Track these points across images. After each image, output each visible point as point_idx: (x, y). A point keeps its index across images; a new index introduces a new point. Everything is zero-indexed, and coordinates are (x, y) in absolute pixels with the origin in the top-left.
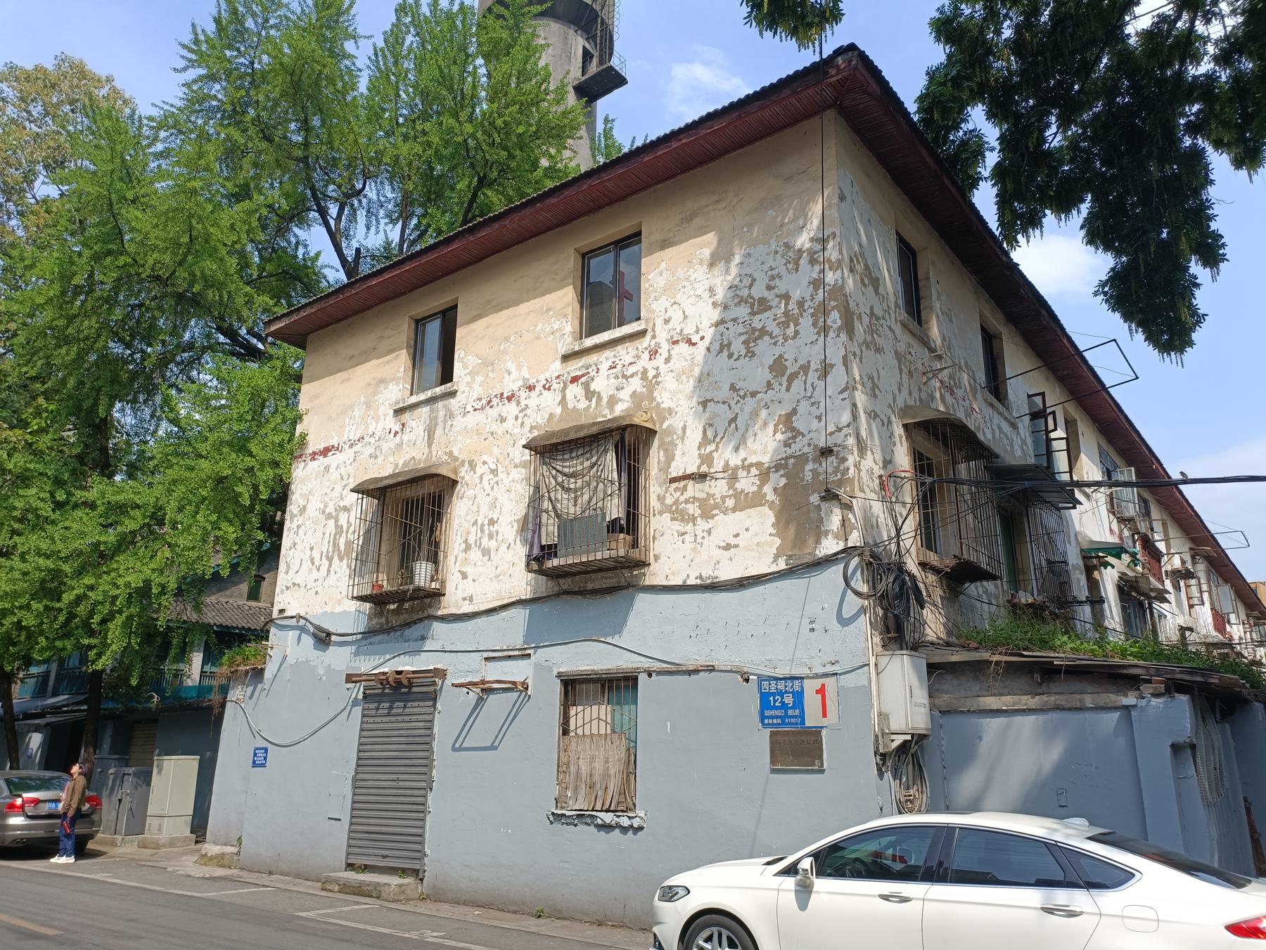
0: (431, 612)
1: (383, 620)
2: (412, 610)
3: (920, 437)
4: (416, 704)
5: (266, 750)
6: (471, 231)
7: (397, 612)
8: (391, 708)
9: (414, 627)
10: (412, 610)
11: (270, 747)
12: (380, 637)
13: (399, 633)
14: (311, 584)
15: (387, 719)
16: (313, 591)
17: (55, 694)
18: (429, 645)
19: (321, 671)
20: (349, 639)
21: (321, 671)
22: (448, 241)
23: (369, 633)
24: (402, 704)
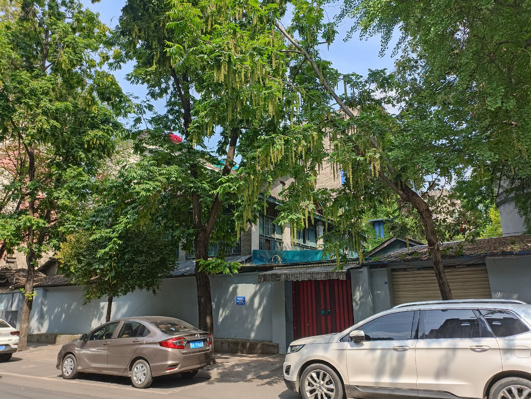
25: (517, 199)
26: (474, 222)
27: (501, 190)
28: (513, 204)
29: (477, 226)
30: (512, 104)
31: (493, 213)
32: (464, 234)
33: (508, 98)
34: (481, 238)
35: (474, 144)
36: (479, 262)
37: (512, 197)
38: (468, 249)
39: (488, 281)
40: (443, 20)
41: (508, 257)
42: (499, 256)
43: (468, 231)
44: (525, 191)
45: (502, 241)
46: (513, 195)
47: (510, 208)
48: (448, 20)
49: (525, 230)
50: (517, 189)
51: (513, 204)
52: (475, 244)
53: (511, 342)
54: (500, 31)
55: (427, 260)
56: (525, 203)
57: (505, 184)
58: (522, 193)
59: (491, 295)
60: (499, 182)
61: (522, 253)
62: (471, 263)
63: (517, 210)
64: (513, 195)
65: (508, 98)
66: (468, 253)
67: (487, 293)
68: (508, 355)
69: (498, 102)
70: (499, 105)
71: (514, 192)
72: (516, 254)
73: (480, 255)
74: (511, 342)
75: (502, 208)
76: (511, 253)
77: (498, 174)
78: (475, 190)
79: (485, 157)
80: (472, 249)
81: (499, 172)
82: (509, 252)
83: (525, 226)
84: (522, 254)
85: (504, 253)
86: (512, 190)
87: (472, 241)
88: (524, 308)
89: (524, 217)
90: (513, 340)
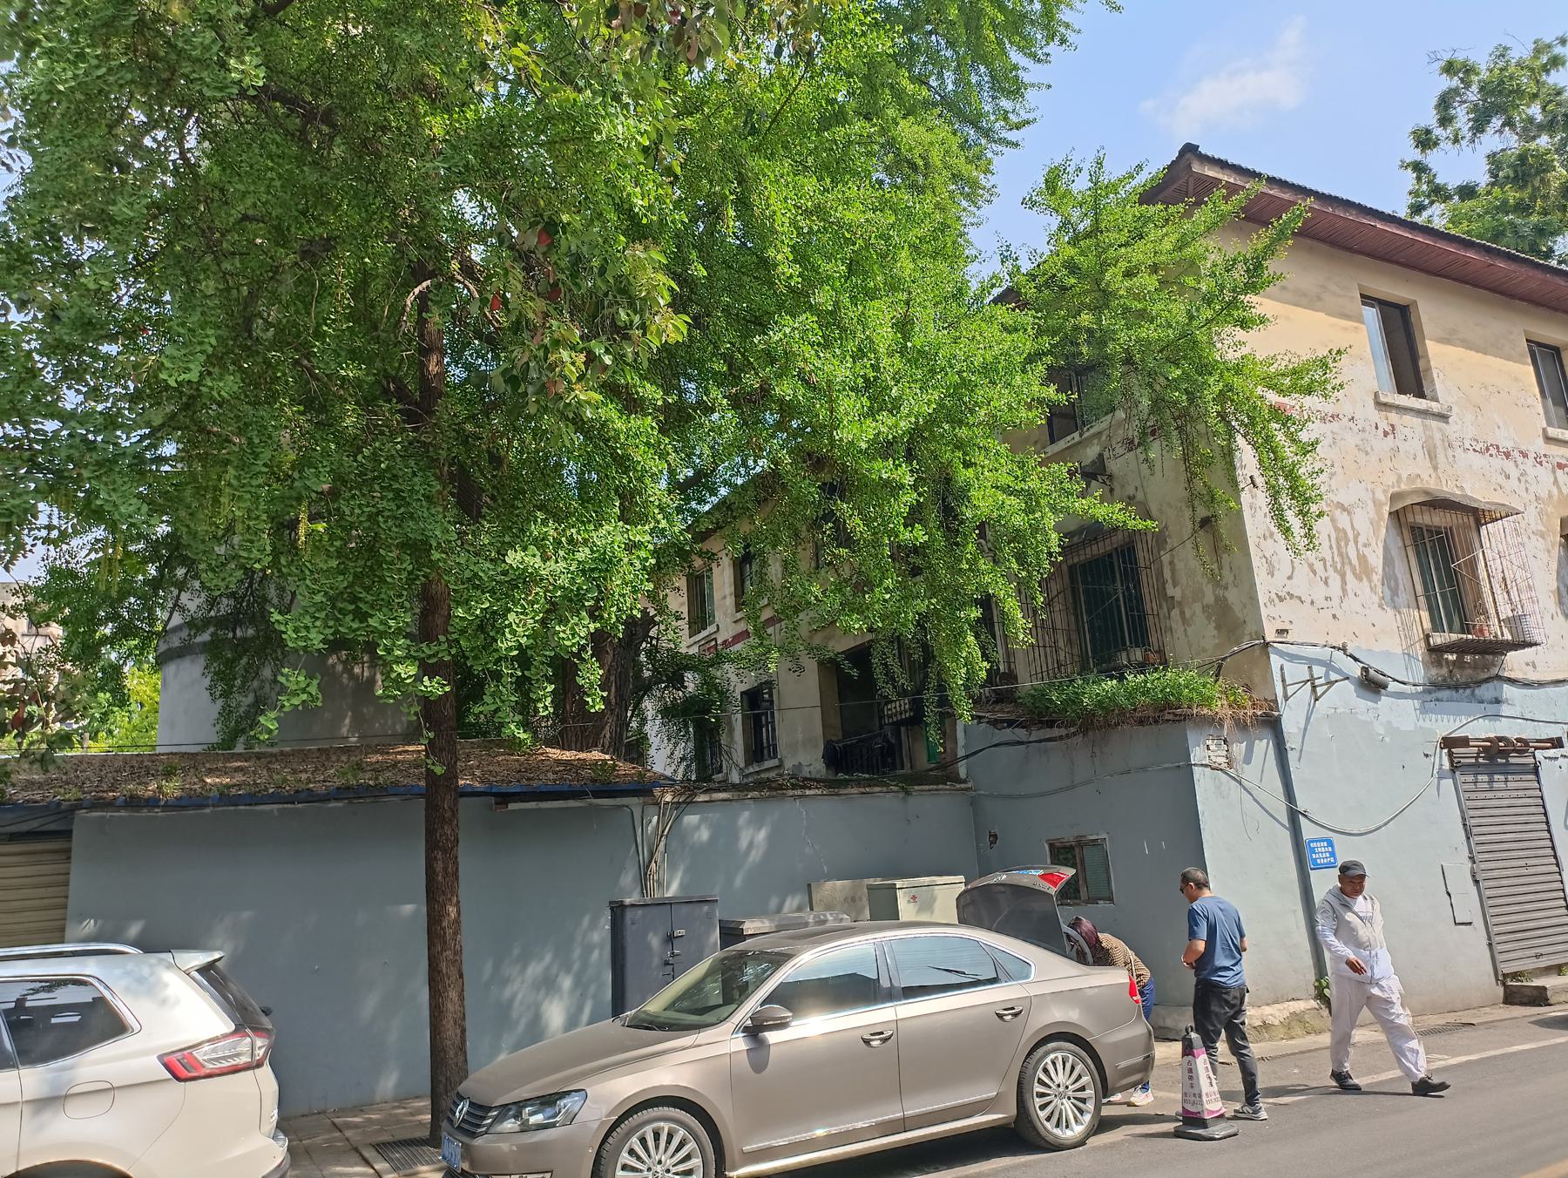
0: (1494, 671)
1: (1444, 671)
2: (1475, 666)
3: (1118, 539)
4: (1517, 777)
5: (1330, 843)
6: (1488, 250)
7: (1460, 664)
8: (1491, 782)
9: (1484, 686)
10: (1475, 666)
11: (1335, 837)
12: (1445, 694)
13: (1468, 691)
14: (1321, 602)
15: (1490, 795)
16: (1329, 613)
17: (671, 969)
18: (1505, 710)
19: (1381, 730)
20: (1408, 689)
21: (1381, 730)
22: (1468, 244)
23: (1435, 686)
24: (1502, 778)
25: (213, 649)
26: (63, 701)
27: (177, 620)
28: (202, 661)
29: (67, 713)
30: (229, 385)
31: (138, 681)
32: (22, 735)
33: (224, 367)
34: (77, 752)
35: (99, 464)
36: (52, 827)
37: (205, 644)
38: (30, 785)
39: (67, 884)
40: (81, 56)
41: (145, 813)
42: (119, 808)
43: (38, 728)
44: (239, 633)
45: (143, 766)
46: (205, 637)
47: (192, 674)
48: (98, 67)
49: (215, 739)
50: (220, 622)
51: (202, 661)
52: (51, 768)
53: (66, 1075)
54: (241, 181)
55: (179, 805)
56: (231, 664)
57: (192, 602)
58: (231, 635)
59: (63, 930)
60: (176, 592)
61: (183, 803)
62: (24, 827)
63: (207, 682)
64: (205, 637)
65: (224, 367)
66: (22, 797)
67: (51, 931)
68: (47, 1116)
69: (191, 366)
70: (193, 376)
71: (212, 629)
72: (167, 807)
73: (59, 804)
74: (66, 1075)
75: (171, 668)
76: (152, 803)
77: (180, 572)
78: (100, 606)
79: (121, 514)
80: (40, 785)
81: (183, 564)
82: (149, 799)
83: (218, 727)
84: (183, 808)
85: (133, 802)
86: (207, 622)
87: (44, 761)
88: (130, 966)
89: (220, 702)
90: (71, 1068)
